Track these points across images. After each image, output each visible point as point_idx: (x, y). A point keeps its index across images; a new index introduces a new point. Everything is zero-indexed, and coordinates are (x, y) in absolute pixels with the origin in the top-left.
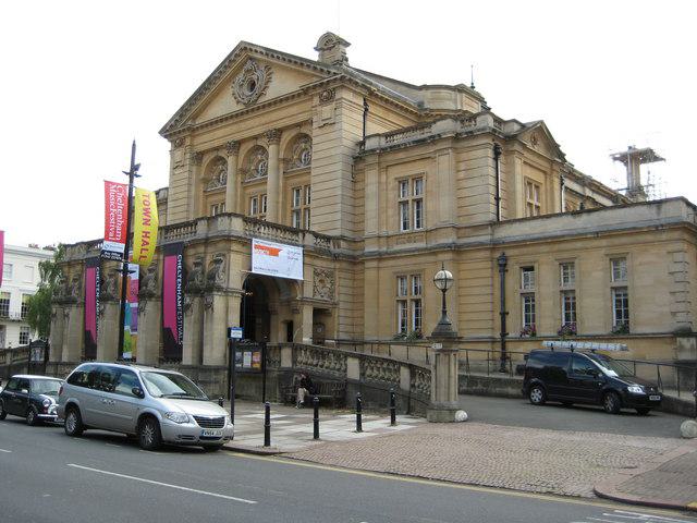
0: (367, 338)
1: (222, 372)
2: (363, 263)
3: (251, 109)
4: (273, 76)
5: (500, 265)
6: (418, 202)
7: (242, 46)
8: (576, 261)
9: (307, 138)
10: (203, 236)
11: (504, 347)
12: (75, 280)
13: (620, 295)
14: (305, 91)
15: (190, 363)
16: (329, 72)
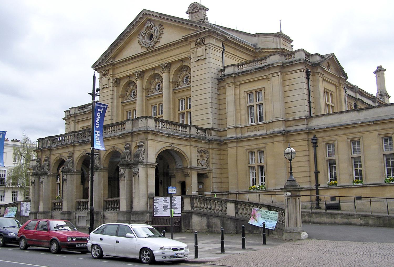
0: (230, 191)
1: (145, 214)
2: (226, 144)
3: (151, 51)
4: (165, 31)
5: (313, 143)
6: (260, 106)
7: (144, 12)
8: (361, 139)
9: (188, 69)
10: (130, 131)
11: (317, 193)
12: (45, 160)
13: (389, 159)
14: (186, 39)
15: (125, 210)
16: (200, 27)
